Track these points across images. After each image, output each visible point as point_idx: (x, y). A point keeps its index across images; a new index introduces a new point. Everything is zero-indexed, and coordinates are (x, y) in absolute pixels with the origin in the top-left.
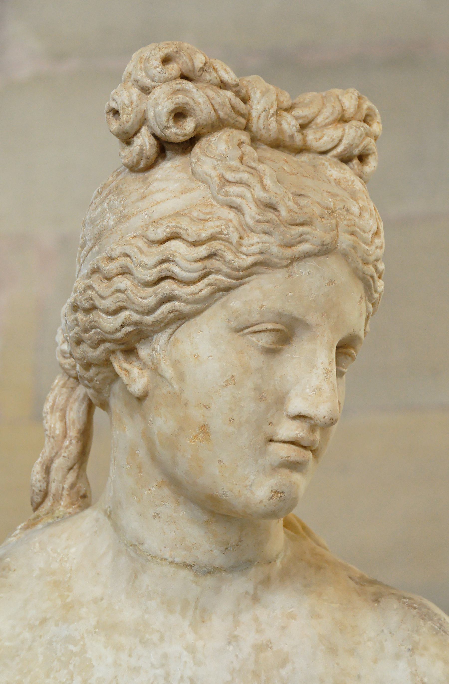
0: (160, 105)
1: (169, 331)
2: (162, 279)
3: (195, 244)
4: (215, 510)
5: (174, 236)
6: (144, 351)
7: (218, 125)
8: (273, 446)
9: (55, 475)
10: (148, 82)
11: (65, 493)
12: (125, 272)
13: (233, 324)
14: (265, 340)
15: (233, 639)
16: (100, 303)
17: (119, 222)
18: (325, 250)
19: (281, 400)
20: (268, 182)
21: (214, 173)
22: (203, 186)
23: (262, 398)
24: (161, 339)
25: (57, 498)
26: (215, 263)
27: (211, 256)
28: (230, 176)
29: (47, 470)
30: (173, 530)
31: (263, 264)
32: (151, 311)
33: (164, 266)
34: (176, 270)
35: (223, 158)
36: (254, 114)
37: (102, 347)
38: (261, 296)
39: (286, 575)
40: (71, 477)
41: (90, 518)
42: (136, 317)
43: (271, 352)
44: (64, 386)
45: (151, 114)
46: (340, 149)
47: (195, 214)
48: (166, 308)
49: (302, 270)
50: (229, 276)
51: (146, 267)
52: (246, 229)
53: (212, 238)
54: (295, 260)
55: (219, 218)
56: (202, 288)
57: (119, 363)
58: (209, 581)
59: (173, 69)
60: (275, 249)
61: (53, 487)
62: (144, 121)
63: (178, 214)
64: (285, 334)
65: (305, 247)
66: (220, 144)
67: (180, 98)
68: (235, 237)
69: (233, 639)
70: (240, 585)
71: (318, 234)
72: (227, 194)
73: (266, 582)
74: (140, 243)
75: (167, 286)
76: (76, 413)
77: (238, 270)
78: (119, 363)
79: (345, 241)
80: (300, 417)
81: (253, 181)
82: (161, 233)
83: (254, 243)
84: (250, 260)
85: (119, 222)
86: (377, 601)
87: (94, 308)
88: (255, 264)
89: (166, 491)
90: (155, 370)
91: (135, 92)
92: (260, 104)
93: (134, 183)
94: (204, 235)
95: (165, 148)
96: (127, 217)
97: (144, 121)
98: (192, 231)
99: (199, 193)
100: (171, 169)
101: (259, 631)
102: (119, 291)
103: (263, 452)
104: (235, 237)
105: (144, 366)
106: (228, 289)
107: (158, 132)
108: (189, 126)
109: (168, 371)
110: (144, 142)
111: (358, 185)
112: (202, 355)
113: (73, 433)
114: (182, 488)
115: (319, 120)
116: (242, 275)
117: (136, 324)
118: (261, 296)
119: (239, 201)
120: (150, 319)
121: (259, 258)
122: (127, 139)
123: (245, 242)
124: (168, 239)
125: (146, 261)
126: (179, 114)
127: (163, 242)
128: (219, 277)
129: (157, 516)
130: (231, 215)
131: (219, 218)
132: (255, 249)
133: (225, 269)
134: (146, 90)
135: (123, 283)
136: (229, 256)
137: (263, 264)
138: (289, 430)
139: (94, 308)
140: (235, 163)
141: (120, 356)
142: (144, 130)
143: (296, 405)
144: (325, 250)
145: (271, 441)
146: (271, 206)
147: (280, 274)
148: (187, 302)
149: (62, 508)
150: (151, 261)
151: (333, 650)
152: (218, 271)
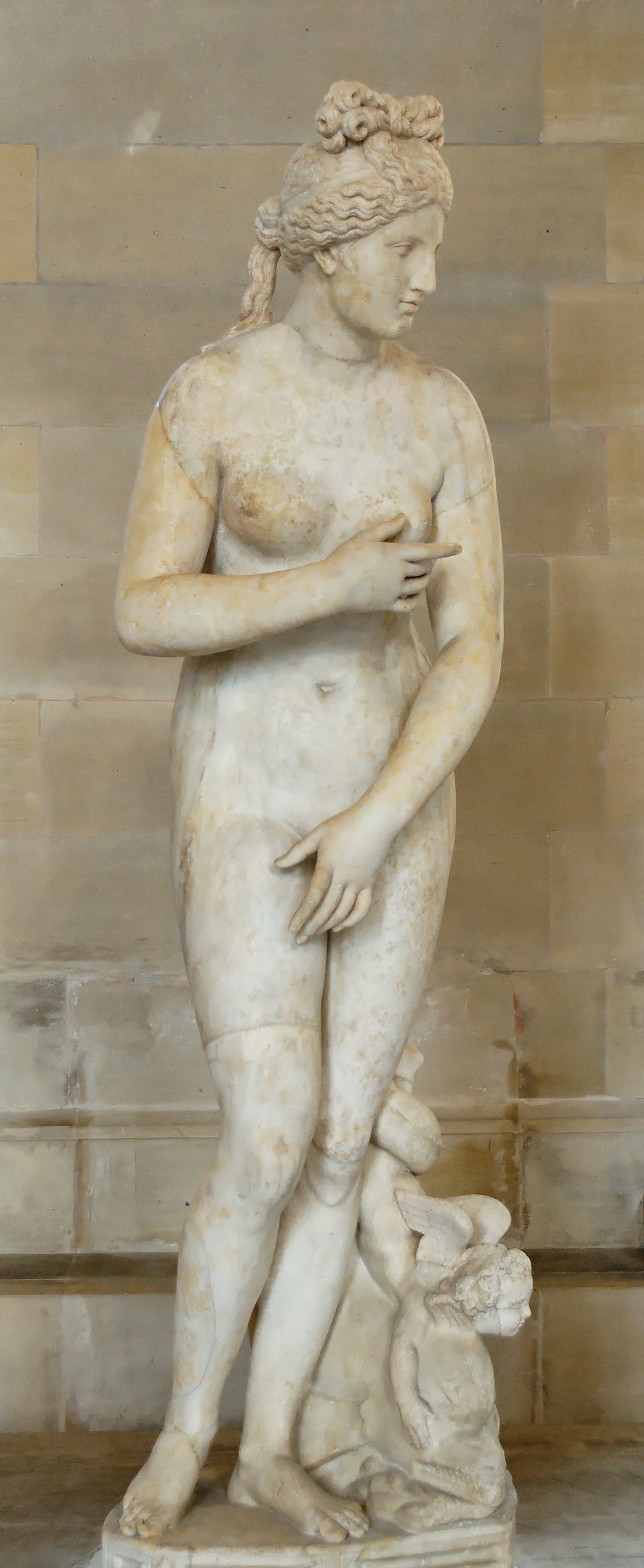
0: (351, 121)
1: (351, 243)
2: (350, 217)
3: (370, 200)
4: (365, 334)
5: (358, 194)
6: (334, 251)
7: (378, 130)
8: (402, 304)
9: (257, 302)
10: (344, 108)
11: (263, 313)
12: (330, 211)
13: (387, 242)
14: (401, 250)
15: (365, 398)
16: (312, 225)
17: (322, 181)
18: (432, 201)
19: (407, 281)
20: (407, 166)
21: (379, 161)
22: (371, 166)
23: (398, 281)
24: (346, 247)
25: (259, 315)
26: (380, 210)
27: (378, 207)
28: (388, 163)
29: (253, 299)
30: (337, 341)
31: (404, 211)
32: (343, 233)
33: (353, 211)
34: (360, 213)
35: (382, 152)
36: (392, 122)
37: (311, 248)
38: (401, 228)
39: (386, 361)
40: (266, 304)
41: (281, 330)
42: (334, 236)
43: (403, 256)
44: (262, 253)
45: (345, 125)
46: (429, 136)
47: (369, 183)
48: (352, 232)
49: (422, 214)
50: (386, 217)
51: (343, 210)
52: (396, 192)
53: (379, 197)
54: (419, 208)
55: (382, 187)
56: (372, 223)
57: (318, 256)
58: (353, 368)
59: (358, 101)
60: (410, 204)
61: (256, 309)
62: (340, 127)
63: (358, 182)
64: (411, 245)
65: (425, 201)
66: (380, 142)
67: (362, 118)
68: (391, 198)
69: (365, 398)
70: (368, 369)
71: (429, 193)
72: (387, 173)
73: (379, 367)
74: (339, 197)
75: (353, 221)
76: (269, 269)
77: (391, 214)
78: (318, 256)
79: (441, 195)
80: (417, 290)
81: (400, 167)
82: (351, 192)
83: (400, 200)
84: (398, 209)
85: (322, 181)
86: (429, 374)
87: (308, 227)
88: (400, 212)
89: (338, 323)
90: (341, 263)
91: (336, 112)
92: (394, 116)
93: (329, 160)
94: (375, 196)
95: (349, 141)
96: (328, 179)
97: (340, 127)
98: (369, 193)
99: (369, 171)
100: (351, 153)
101: (377, 393)
102: (326, 221)
103: (397, 307)
104: (391, 198)
105: (333, 258)
106: (385, 224)
107: (348, 134)
108: (364, 132)
109: (349, 264)
110: (339, 139)
111: (436, 152)
112: (369, 257)
113: (269, 280)
114: (348, 322)
115: (418, 118)
116: (392, 217)
117: (332, 238)
118: (401, 228)
119: (392, 177)
120: (342, 237)
121: (402, 208)
122: (329, 136)
123: (396, 200)
124: (354, 196)
125: (343, 207)
126: (360, 126)
127: (351, 197)
128: (381, 217)
129: (331, 335)
130: (389, 185)
131: (382, 187)
132: (401, 204)
133: (385, 214)
134: (342, 112)
135: (330, 217)
136: (388, 207)
137: (404, 211)
138: (411, 296)
139: (308, 227)
140: (390, 156)
141: (320, 252)
142: (340, 133)
143: (415, 283)
144: (432, 201)
145: (401, 302)
146: (409, 181)
147: (411, 217)
148: (364, 230)
149: (262, 320)
150: (346, 207)
151: (412, 402)
152: (381, 215)
